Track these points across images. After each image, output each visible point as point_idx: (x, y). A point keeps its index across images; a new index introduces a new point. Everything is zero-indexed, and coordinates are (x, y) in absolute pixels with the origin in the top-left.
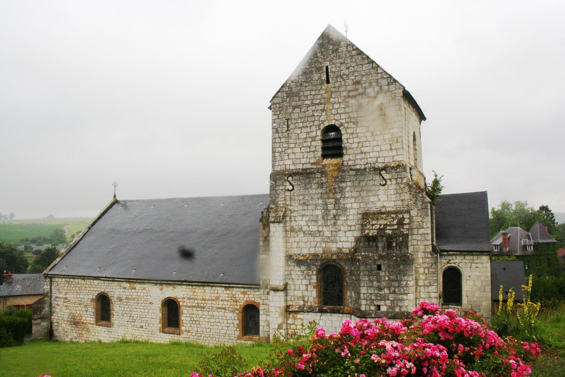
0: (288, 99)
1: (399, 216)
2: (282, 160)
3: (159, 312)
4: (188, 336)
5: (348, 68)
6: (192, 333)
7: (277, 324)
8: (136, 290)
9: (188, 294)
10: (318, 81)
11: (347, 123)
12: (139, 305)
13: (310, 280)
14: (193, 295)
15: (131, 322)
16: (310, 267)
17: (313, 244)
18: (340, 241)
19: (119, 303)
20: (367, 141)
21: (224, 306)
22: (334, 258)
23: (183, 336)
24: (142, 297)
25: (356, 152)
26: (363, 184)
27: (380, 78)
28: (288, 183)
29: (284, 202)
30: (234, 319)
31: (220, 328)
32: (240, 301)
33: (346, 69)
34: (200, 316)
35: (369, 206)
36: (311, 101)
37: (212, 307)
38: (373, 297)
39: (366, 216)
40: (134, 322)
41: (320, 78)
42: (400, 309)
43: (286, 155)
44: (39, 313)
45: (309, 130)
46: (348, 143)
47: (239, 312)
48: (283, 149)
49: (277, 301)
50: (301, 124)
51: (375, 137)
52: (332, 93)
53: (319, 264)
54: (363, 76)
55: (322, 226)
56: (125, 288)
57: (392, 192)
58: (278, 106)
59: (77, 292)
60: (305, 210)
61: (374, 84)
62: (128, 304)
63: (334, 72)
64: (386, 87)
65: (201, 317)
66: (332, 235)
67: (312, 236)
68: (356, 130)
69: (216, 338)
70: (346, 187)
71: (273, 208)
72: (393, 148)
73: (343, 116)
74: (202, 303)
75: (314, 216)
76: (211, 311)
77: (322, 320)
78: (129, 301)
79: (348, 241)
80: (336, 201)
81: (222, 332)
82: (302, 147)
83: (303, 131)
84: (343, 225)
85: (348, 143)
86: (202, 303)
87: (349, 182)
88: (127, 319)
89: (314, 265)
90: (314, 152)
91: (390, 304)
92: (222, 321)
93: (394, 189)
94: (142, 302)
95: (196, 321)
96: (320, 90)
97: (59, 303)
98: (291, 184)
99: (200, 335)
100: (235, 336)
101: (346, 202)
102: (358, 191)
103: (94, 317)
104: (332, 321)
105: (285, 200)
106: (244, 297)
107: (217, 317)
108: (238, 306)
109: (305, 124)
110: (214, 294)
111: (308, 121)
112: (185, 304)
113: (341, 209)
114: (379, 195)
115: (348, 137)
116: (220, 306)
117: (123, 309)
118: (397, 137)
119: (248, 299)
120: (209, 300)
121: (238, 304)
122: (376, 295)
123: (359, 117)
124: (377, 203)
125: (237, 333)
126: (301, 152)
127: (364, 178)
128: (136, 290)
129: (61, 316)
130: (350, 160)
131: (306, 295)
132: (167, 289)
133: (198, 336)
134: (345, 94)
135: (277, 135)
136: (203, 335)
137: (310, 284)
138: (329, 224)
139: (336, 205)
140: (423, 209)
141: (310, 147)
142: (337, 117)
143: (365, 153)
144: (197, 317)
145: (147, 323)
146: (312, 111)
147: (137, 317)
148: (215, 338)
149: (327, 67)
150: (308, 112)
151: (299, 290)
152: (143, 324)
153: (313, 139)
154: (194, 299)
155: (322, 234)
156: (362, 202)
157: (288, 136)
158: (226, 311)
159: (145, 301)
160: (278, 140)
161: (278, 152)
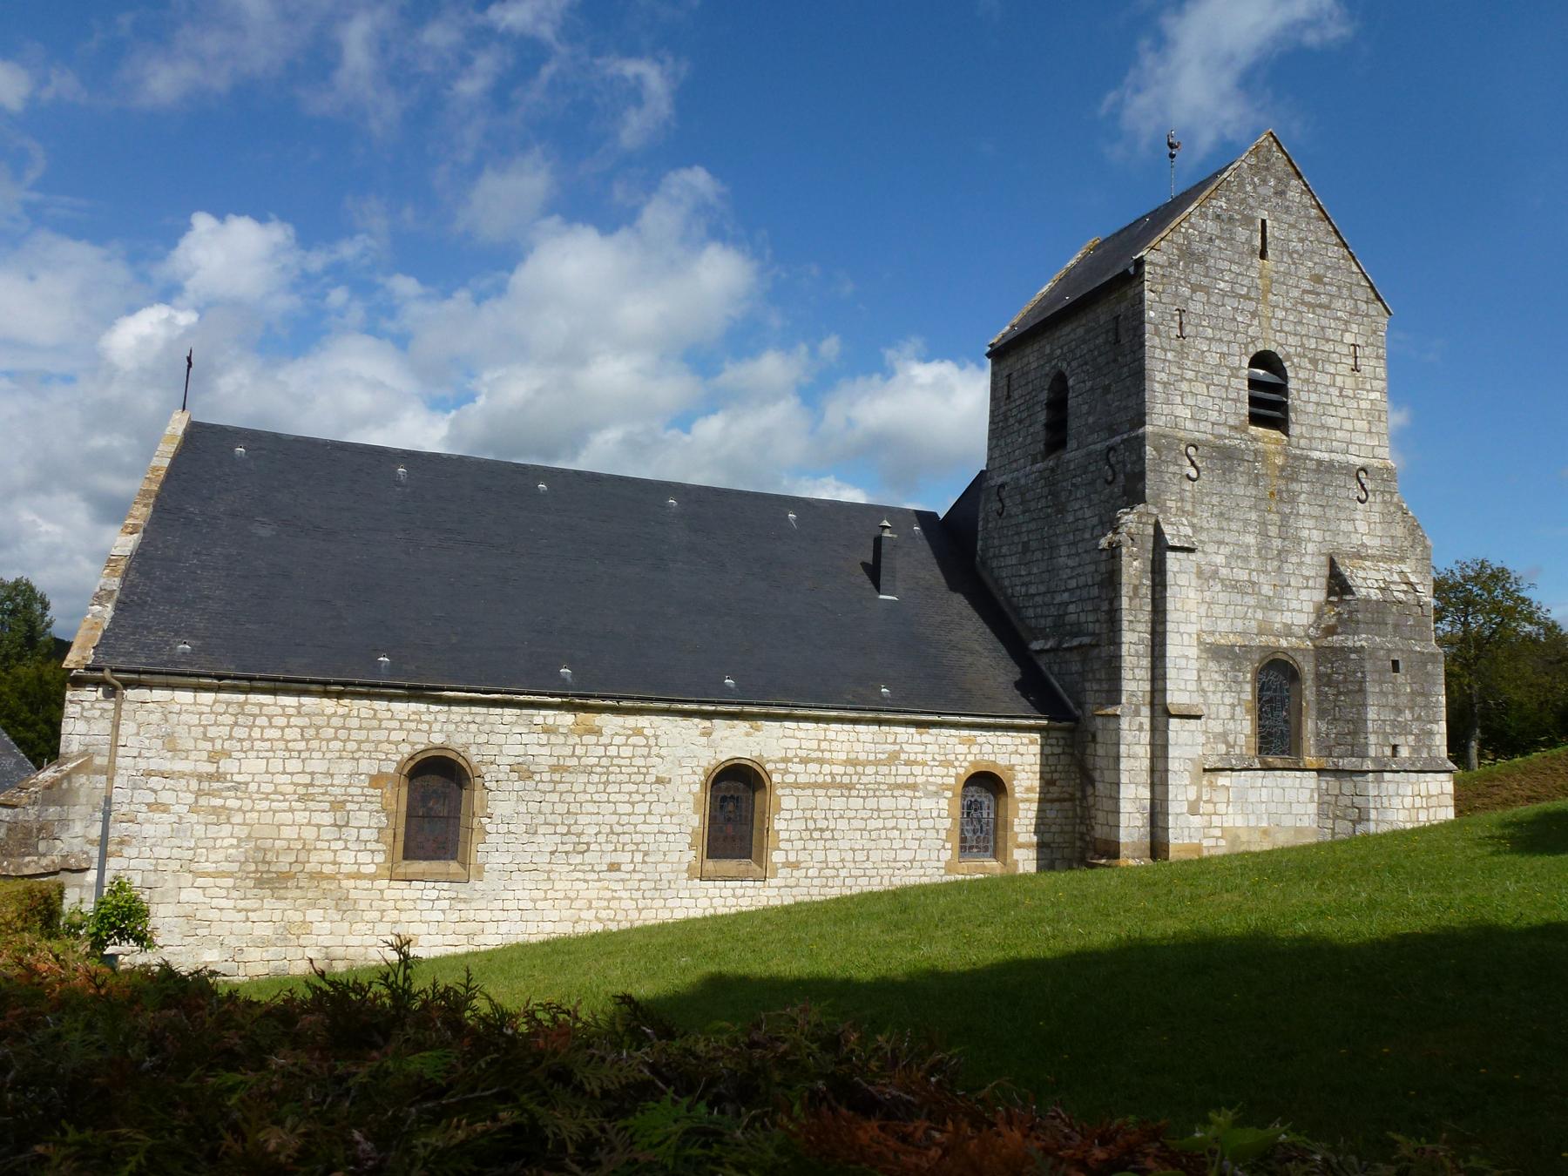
0: (1181, 263)
2: (1168, 402)
4: (792, 882)
6: (808, 869)
8: (602, 735)
9: (800, 748)
10: (1246, 246)
11: (1298, 355)
13: (1239, 693)
14: (819, 749)
16: (1240, 663)
18: (1288, 610)
19: (518, 785)
20: (1332, 404)
21: (911, 780)
23: (773, 882)
25: (1313, 423)
26: (1330, 491)
29: (1179, 504)
30: (939, 816)
31: (897, 844)
35: (1341, 539)
38: (1388, 729)
40: (583, 853)
41: (1249, 241)
43: (1177, 392)
44: (42, 846)
45: (1225, 349)
46: (1300, 399)
47: (954, 796)
49: (1186, 745)
50: (1210, 331)
52: (1272, 282)
53: (1257, 657)
55: (1257, 571)
56: (548, 730)
57: (1376, 518)
59: (287, 749)
60: (1222, 529)
62: (560, 787)
66: (1275, 593)
68: (1314, 375)
69: (882, 877)
70: (1300, 493)
72: (1374, 430)
73: (1291, 340)
74: (845, 774)
75: (1241, 546)
78: (568, 777)
80: (1282, 521)
81: (904, 855)
84: (1294, 574)
85: (1300, 399)
86: (845, 774)
87: (1307, 482)
88: (546, 842)
89: (1247, 659)
91: (1413, 743)
92: (902, 824)
94: (625, 778)
95: (822, 830)
97: (166, 797)
98: (1193, 463)
99: (833, 872)
102: (1321, 506)
103: (380, 846)
105: (1182, 500)
106: (970, 753)
107: (889, 814)
108: (951, 776)
110: (884, 746)
112: (790, 779)
116: (900, 780)
117: (534, 807)
118: (1379, 411)
119: (978, 757)
120: (870, 763)
122: (1394, 724)
125: (946, 855)
128: (602, 735)
130: (1302, 436)
132: (727, 733)
133: (827, 878)
134: (1296, 293)
136: (843, 873)
137: (1239, 704)
138: (1269, 568)
139: (1282, 528)
141: (1227, 388)
143: (1328, 429)
144: (826, 819)
145: (638, 850)
146: (1233, 308)
147: (599, 832)
149: (1264, 222)
151: (1218, 718)
152: (624, 858)
154: (821, 761)
157: (1182, 349)
158: (917, 794)
159: (639, 773)
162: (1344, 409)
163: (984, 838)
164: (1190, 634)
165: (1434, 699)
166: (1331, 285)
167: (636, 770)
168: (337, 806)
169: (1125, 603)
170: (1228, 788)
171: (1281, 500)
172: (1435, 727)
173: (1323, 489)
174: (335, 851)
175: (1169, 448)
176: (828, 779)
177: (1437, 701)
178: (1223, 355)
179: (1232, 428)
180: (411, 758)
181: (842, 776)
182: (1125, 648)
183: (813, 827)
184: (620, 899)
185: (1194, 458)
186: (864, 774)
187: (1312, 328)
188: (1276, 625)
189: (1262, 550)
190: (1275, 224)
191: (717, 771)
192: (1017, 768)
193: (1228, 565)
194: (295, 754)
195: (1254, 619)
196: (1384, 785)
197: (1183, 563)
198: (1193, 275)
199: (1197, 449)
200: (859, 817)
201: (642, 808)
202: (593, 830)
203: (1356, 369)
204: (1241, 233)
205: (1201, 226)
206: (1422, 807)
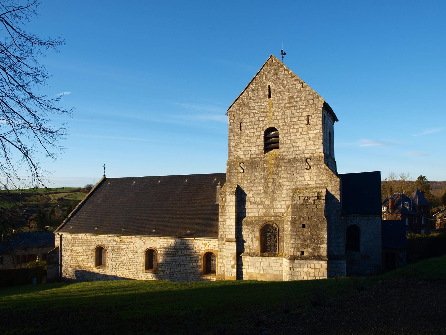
6: (167, 272)
7: (231, 265)
11: (283, 125)
15: (121, 265)
18: (276, 208)
24: (130, 248)
25: (289, 146)
28: (240, 168)
29: (237, 181)
35: (298, 183)
42: (318, 254)
43: (238, 148)
45: (255, 131)
49: (231, 249)
50: (250, 126)
53: (261, 224)
56: (116, 242)
57: (314, 174)
62: (119, 253)
67: (256, 205)
70: (281, 171)
72: (316, 143)
74: (174, 251)
76: (181, 257)
77: (262, 262)
80: (274, 181)
85: (283, 140)
95: (169, 264)
97: (67, 253)
100: (198, 274)
101: (281, 181)
103: (93, 262)
106: (205, 247)
116: (187, 253)
124: (303, 182)
130: (284, 152)
131: (251, 245)
136: (175, 274)
137: (254, 237)
138: (268, 196)
141: (256, 143)
143: (295, 147)
148: (183, 276)
149: (269, 86)
157: (240, 134)
159: (132, 250)
161: (233, 146)
162: (302, 139)
164: (233, 219)
165: (321, 236)
166: (297, 98)
167: (132, 249)
168: (87, 255)
169: (220, 211)
170: (248, 262)
172: (321, 246)
173: (291, 168)
174: (87, 263)
175: (234, 165)
177: (323, 237)
179: (257, 154)
180: (96, 247)
181: (173, 252)
183: (167, 263)
184: (131, 275)
187: (288, 115)
188: (271, 213)
190: (274, 85)
191: (147, 250)
193: (253, 197)
194: (81, 246)
196: (294, 264)
199: (243, 164)
200: (178, 261)
201: (133, 257)
202: (125, 261)
204: (261, 92)
205: (247, 95)
206: (312, 272)
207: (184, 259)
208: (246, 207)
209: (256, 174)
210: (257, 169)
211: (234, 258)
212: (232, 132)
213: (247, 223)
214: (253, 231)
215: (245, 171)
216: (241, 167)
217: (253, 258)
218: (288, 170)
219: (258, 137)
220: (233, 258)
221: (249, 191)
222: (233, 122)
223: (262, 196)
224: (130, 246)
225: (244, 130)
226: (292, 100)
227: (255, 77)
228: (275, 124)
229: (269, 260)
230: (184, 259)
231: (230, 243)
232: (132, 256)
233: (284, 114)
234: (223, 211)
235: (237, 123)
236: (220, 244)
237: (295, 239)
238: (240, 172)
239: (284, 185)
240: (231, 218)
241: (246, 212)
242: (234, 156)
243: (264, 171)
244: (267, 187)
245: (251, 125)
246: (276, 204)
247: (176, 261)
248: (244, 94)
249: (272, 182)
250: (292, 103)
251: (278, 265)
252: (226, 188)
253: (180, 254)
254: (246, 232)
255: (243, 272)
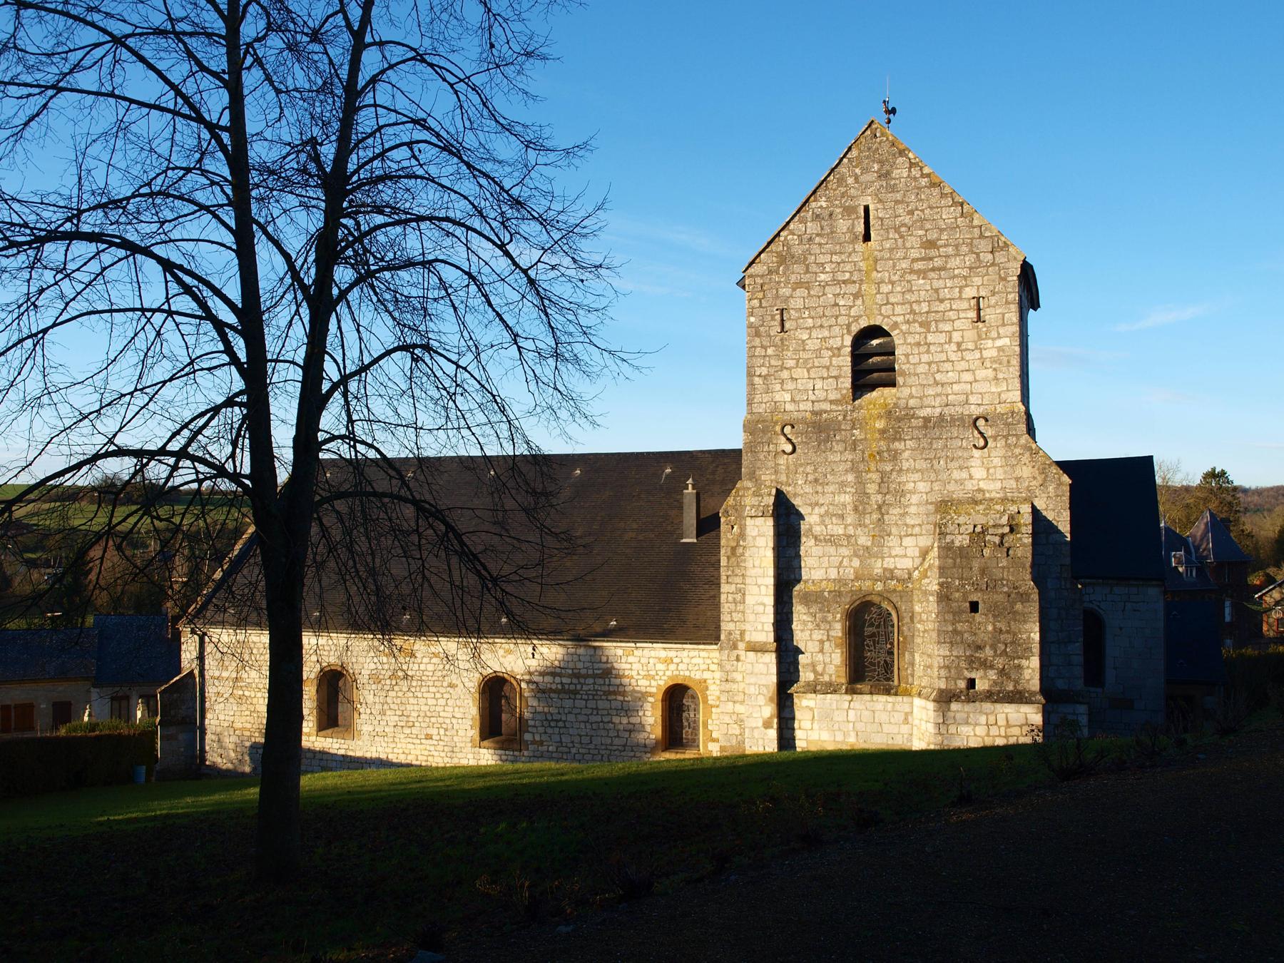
0: (781, 268)
1: (1011, 508)
3: (471, 704)
5: (911, 213)
6: (549, 746)
11: (908, 322)
12: (424, 689)
15: (402, 727)
17: (835, 561)
18: (890, 556)
19: (374, 687)
20: (948, 360)
22: (879, 589)
25: (925, 382)
27: (976, 236)
28: (783, 439)
29: (773, 477)
32: (657, 677)
33: (908, 214)
34: (566, 711)
35: (951, 487)
36: (831, 275)
37: (594, 690)
39: (945, 506)
41: (851, 230)
42: (1015, 686)
43: (777, 381)
45: (826, 333)
48: (772, 370)
49: (761, 674)
50: (810, 321)
51: (964, 353)
52: (876, 261)
53: (848, 600)
54: (942, 230)
57: (997, 462)
58: (759, 281)
60: (817, 492)
61: (964, 249)
63: (882, 219)
64: (990, 256)
65: (570, 713)
68: (926, 338)
69: (602, 756)
70: (904, 451)
71: (749, 489)
72: (1000, 376)
73: (898, 309)
74: (571, 683)
76: (593, 699)
79: (905, 556)
80: (882, 478)
82: (811, 368)
83: (814, 334)
85: (908, 362)
87: (910, 440)
90: (836, 378)
93: (1001, 457)
95: (557, 721)
96: (850, 254)
101: (904, 479)
104: (873, 711)
107: (606, 712)
109: (819, 322)
111: (824, 315)
113: (891, 491)
114: (972, 467)
115: (909, 351)
119: (675, 673)
121: (652, 685)
123: (932, 312)
124: (966, 482)
126: (809, 378)
127: (941, 434)
129: (227, 718)
130: (911, 396)
133: (562, 753)
134: (904, 265)
135: (757, 341)
136: (574, 751)
137: (828, 640)
138: (867, 521)
140: (1057, 496)
141: (828, 368)
142: (886, 310)
143: (943, 385)
144: (559, 713)
147: (419, 716)
148: (600, 756)
149: (867, 209)
150: (824, 297)
152: (434, 732)
153: (837, 352)
155: (853, 540)
156: (936, 481)
157: (782, 343)
160: (758, 351)
161: (760, 376)
162: (963, 363)
163: (692, 733)
164: (767, 586)
166: (945, 246)
169: (723, 562)
170: (811, 709)
171: (881, 460)
175: (764, 431)
176: (559, 687)
177: (1029, 637)
178: (824, 339)
179: (831, 402)
181: (569, 684)
182: (723, 597)
185: (789, 436)
186: (585, 684)
187: (923, 293)
188: (876, 571)
189: (860, 508)
192: (708, 681)
193: (823, 523)
195: (851, 567)
197: (761, 529)
198: (793, 276)
199: (793, 427)
201: (442, 702)
203: (979, 319)
207: (601, 704)
208: (802, 553)
209: (831, 457)
210: (834, 444)
211: (771, 699)
212: (758, 334)
213: (806, 599)
214: (824, 620)
215: (797, 447)
216: (785, 435)
217: (825, 699)
218: (924, 448)
219: (836, 351)
220: (768, 699)
221: (810, 505)
222: (761, 306)
223: (849, 520)
224: (430, 667)
225: (792, 332)
226: (933, 253)
227: (825, 180)
228: (885, 317)
229: (872, 703)
230: (601, 704)
231: (759, 654)
232: (437, 699)
233: (910, 291)
234: (735, 564)
235: (773, 311)
236: (725, 657)
237: (951, 642)
238: (784, 451)
239: (913, 492)
240: (759, 583)
241: (803, 565)
242: (765, 403)
243: (855, 450)
244: (862, 496)
245: (813, 318)
246: (891, 544)
247: (578, 711)
248: (792, 226)
249: (879, 480)
250: (931, 259)
251: (899, 717)
252: (741, 496)
253: (589, 690)
254: (805, 623)
255: (797, 738)
